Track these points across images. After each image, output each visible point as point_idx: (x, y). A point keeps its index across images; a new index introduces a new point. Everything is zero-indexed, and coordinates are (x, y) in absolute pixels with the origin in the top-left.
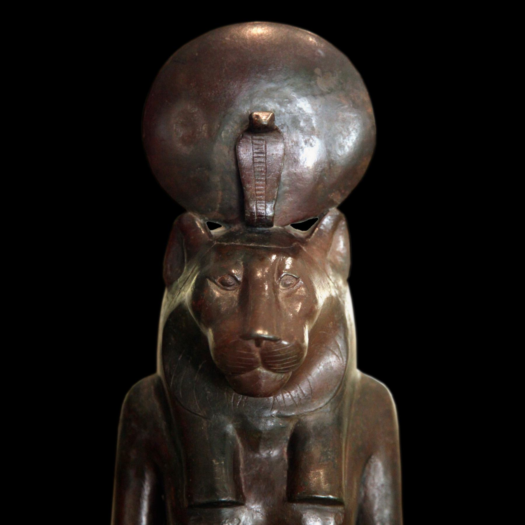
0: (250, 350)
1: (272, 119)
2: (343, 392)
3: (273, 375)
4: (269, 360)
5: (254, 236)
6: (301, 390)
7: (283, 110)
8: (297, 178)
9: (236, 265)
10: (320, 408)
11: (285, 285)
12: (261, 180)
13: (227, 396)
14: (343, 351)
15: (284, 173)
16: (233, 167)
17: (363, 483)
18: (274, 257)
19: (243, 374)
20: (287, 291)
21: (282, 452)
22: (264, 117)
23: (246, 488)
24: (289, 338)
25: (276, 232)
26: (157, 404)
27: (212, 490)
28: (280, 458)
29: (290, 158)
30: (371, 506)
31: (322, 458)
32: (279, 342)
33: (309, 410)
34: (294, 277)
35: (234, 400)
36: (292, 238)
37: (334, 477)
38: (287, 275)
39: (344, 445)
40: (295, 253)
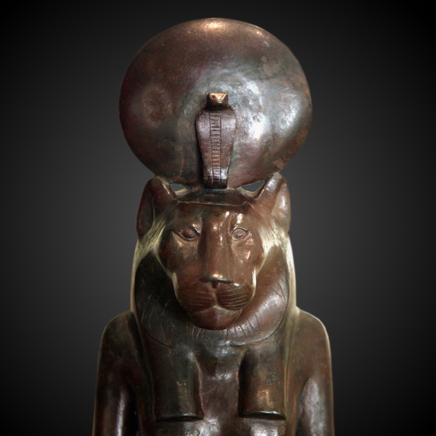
0: (207, 291)
1: (226, 99)
2: (285, 325)
3: (227, 311)
4: (223, 299)
5: (211, 196)
6: (250, 324)
7: (235, 91)
8: (247, 148)
9: (196, 220)
10: (266, 339)
11: (237, 237)
12: (217, 150)
13: (189, 329)
14: (285, 292)
15: (236, 143)
16: (194, 139)
17: (301, 401)
18: (227, 214)
19: (202, 310)
20: (238, 242)
21: (234, 375)
22: (219, 98)
23: (204, 405)
24: (240, 281)
25: (230, 192)
26: (131, 336)
27: (176, 407)
28: (233, 381)
29: (241, 131)
30: (309, 420)
31: (268, 380)
32: (231, 284)
33: (257, 340)
34: (244, 230)
35: (194, 332)
36: (242, 198)
37: (277, 396)
38: (238, 228)
39: (285, 370)
40: (245, 210)
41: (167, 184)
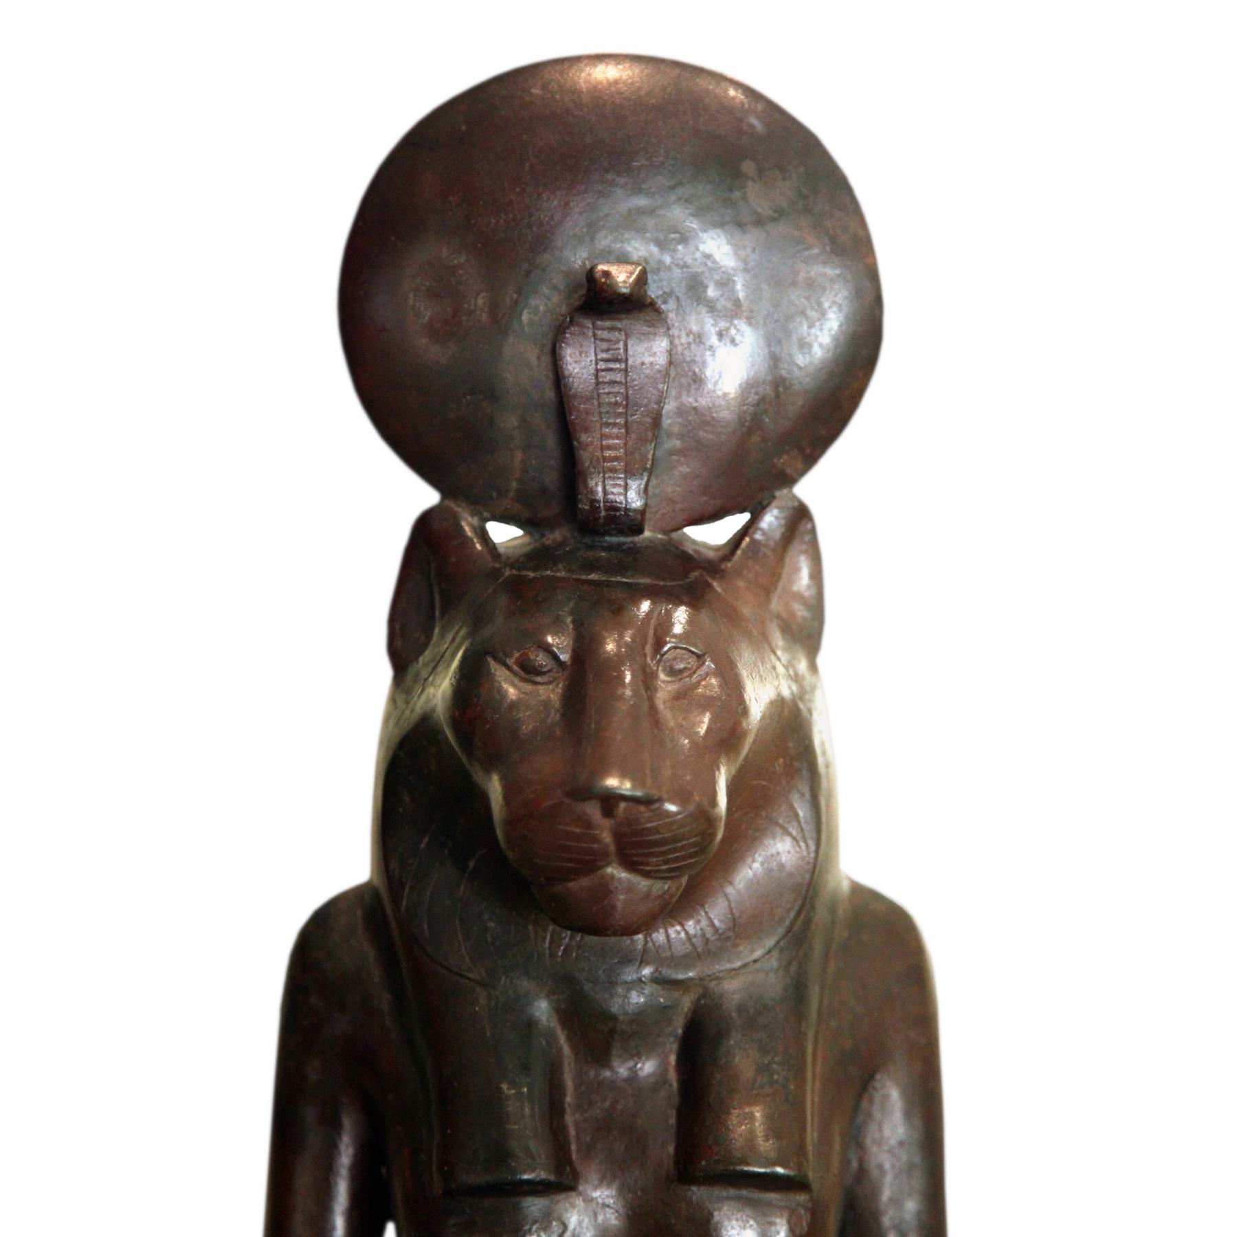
0: (588, 824)
1: (642, 280)
2: (808, 923)
3: (643, 883)
4: (634, 848)
6: (710, 919)
7: (667, 259)
8: (700, 419)
9: (556, 625)
10: (755, 961)
11: (672, 672)
12: (615, 425)
13: (536, 932)
14: (809, 828)
15: (670, 407)
16: (550, 394)
17: (855, 1139)
18: (645, 606)
19: (572, 880)
20: (676, 686)
21: (664, 1065)
22: (623, 277)
23: (579, 1149)
24: (681, 797)
25: (651, 546)
26: (370, 953)
27: (500, 1155)
28: (660, 1080)
29: (684, 372)
30: (875, 1193)
31: (759, 1079)
32: (657, 805)
33: (728, 966)
34: (692, 652)
35: (552, 941)
37: (786, 1124)
38: (676, 648)
39: (810, 1049)
40: (695, 596)
41: (475, 521)
